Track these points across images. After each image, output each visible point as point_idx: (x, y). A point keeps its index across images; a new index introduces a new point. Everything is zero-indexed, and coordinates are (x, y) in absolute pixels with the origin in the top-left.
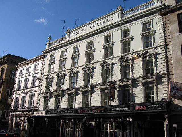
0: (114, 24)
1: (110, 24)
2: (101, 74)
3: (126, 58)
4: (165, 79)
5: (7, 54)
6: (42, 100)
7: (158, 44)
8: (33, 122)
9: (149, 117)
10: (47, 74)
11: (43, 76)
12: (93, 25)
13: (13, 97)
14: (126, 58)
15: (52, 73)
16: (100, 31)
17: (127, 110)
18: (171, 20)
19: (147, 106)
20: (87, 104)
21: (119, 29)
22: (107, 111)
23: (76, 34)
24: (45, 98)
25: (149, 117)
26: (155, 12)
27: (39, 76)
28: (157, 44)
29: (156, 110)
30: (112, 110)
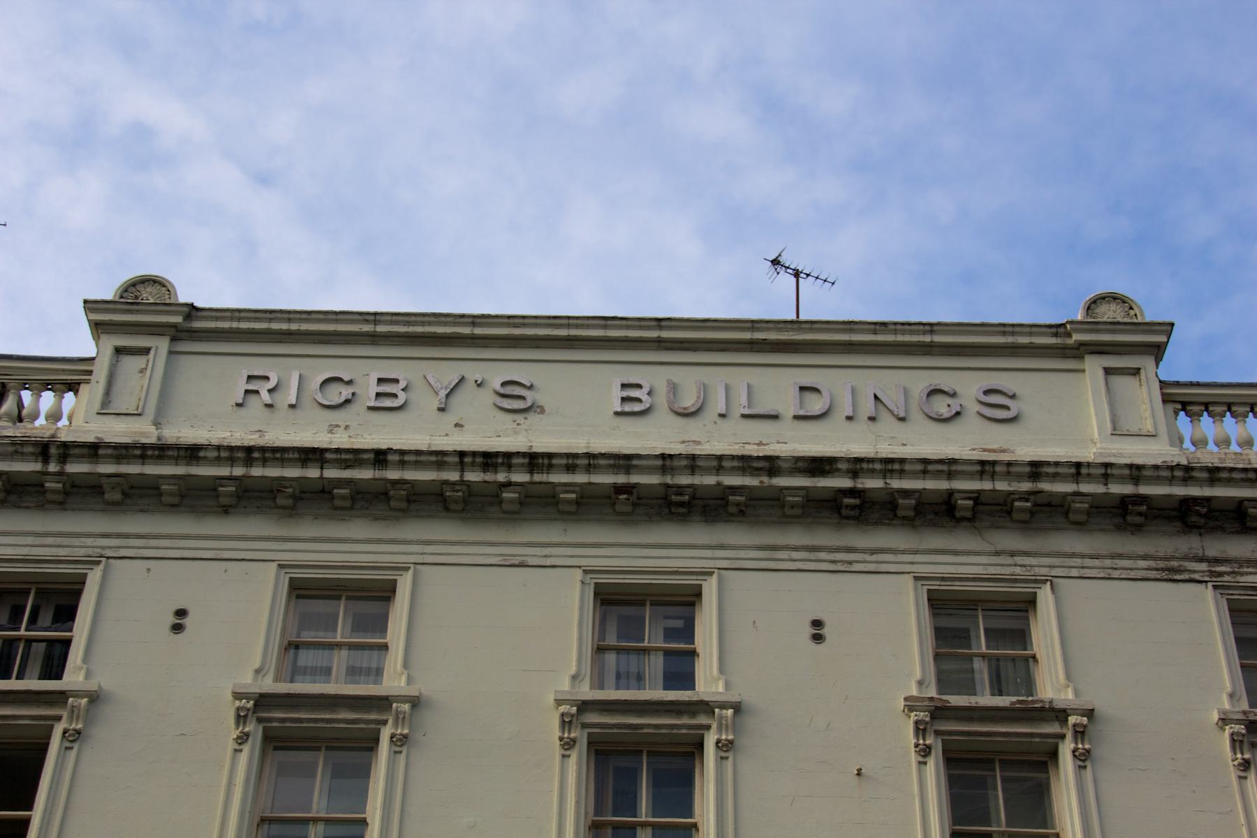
16: (852, 492)
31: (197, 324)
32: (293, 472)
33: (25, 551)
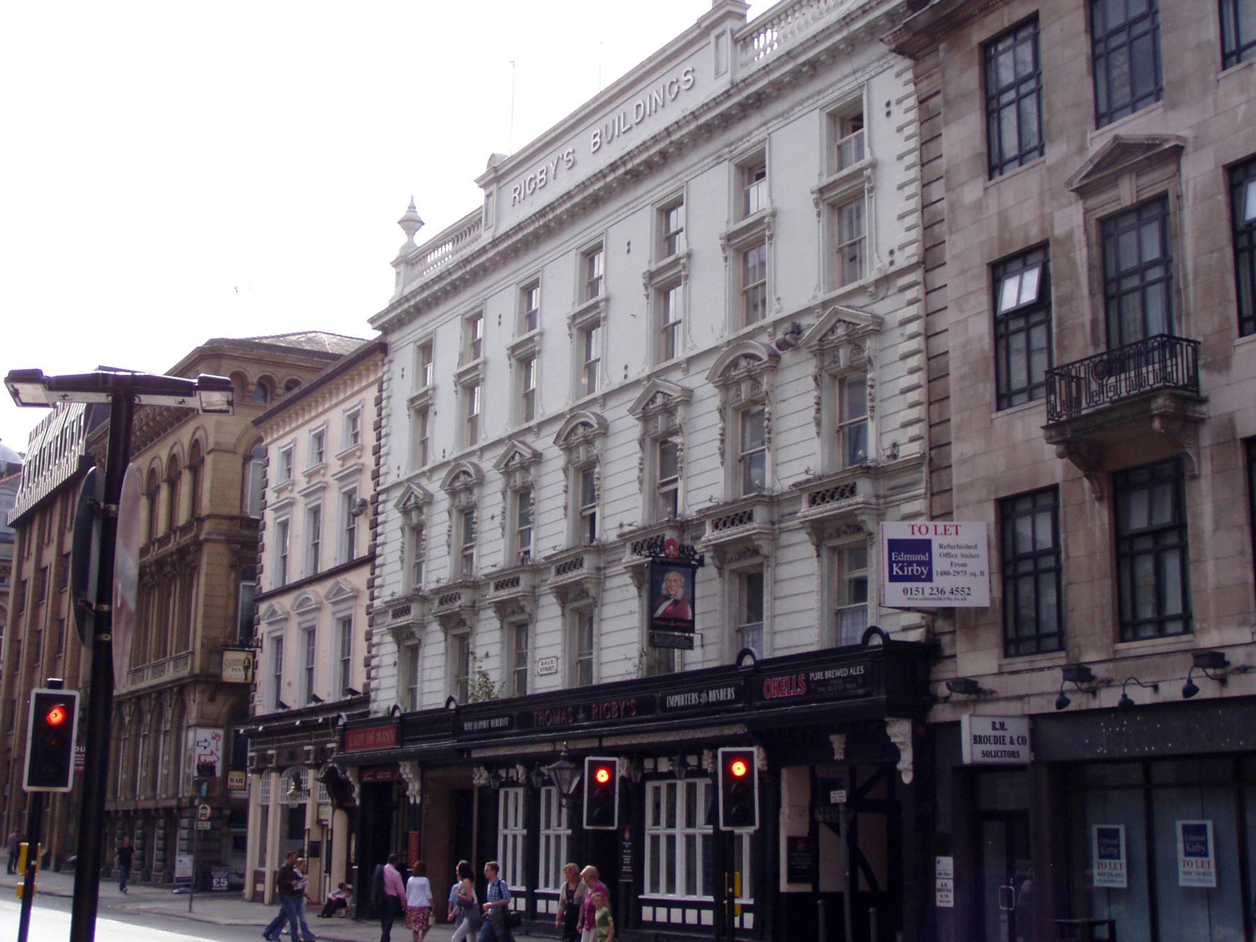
0: (647, 149)
1: (519, 225)
2: (635, 473)
3: (743, 363)
4: (915, 498)
5: (201, 342)
6: (388, 651)
7: (892, 263)
8: (365, 787)
9: (838, 743)
10: (640, 368)
11: (387, 490)
12: (666, 81)
13: (259, 636)
14: (743, 363)
15: (680, 354)
17: (731, 702)
18: (951, 90)
19: (470, 724)
20: (586, 667)
21: (719, 160)
22: (652, 711)
23: (668, 98)
24: (401, 635)
25: (838, 743)
26: (853, 45)
27: (366, 490)
28: (887, 259)
29: (567, 730)
30: (676, 700)
31: (500, 173)
32: (505, 245)
33: (673, 187)
